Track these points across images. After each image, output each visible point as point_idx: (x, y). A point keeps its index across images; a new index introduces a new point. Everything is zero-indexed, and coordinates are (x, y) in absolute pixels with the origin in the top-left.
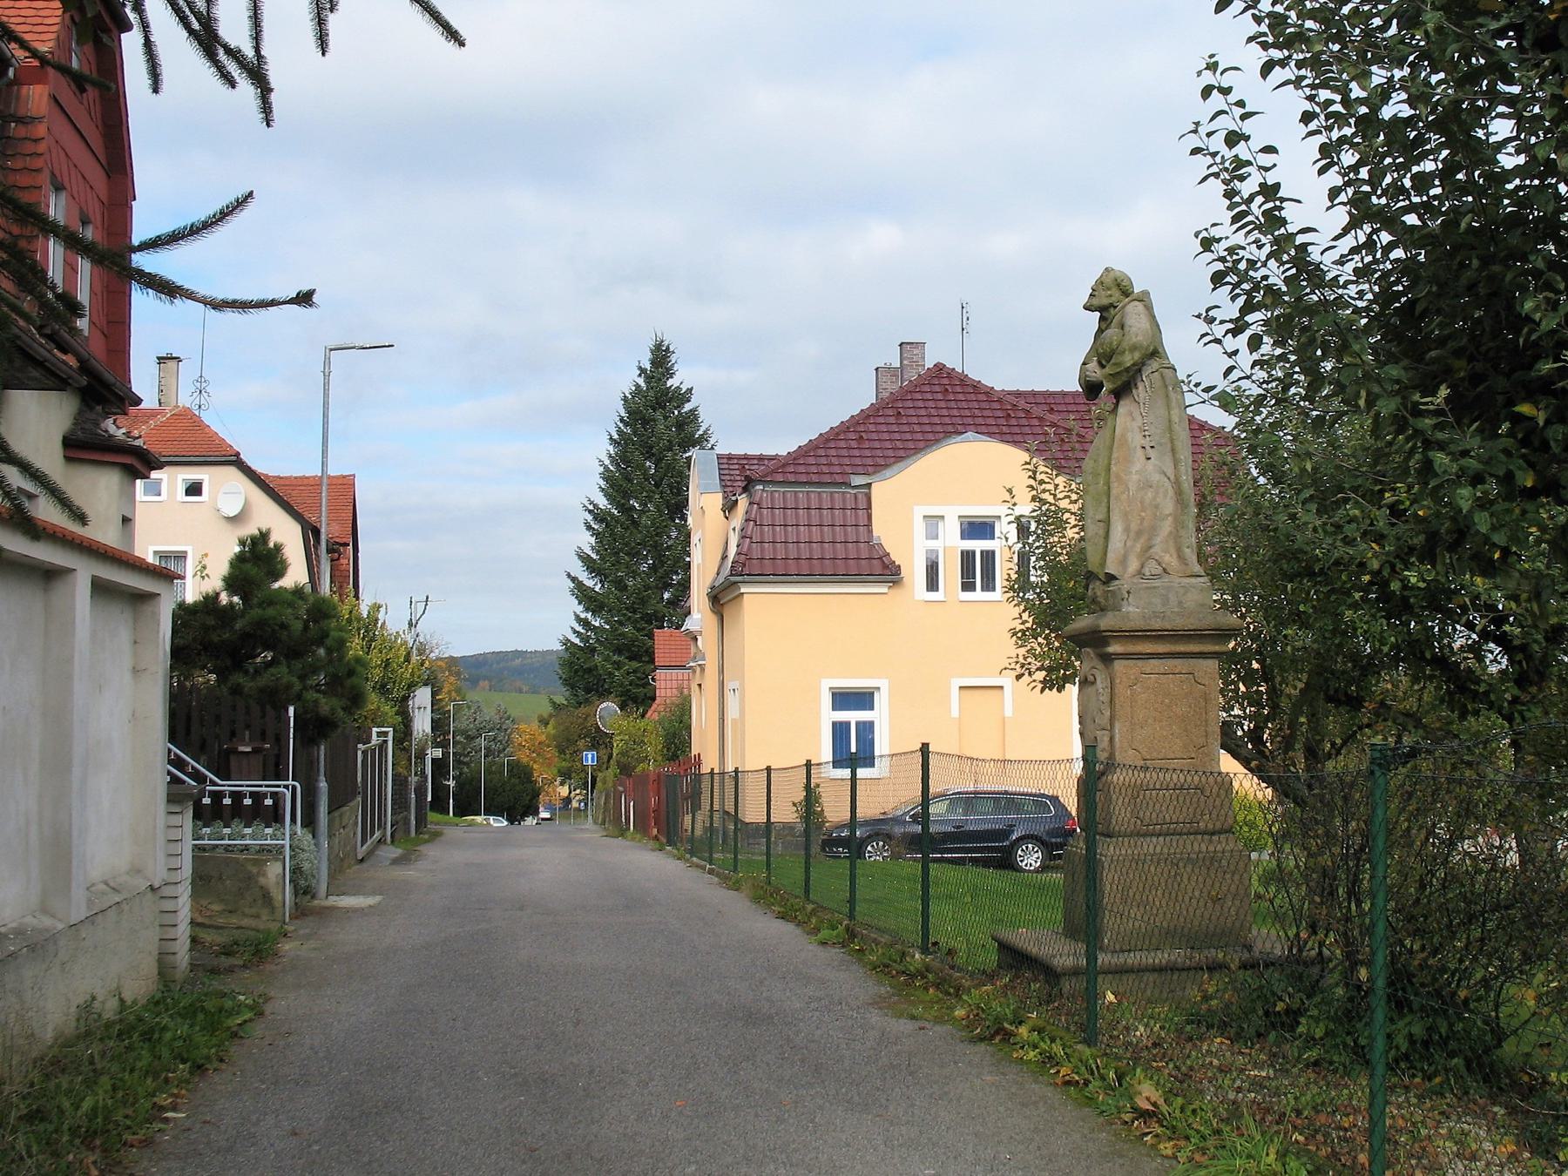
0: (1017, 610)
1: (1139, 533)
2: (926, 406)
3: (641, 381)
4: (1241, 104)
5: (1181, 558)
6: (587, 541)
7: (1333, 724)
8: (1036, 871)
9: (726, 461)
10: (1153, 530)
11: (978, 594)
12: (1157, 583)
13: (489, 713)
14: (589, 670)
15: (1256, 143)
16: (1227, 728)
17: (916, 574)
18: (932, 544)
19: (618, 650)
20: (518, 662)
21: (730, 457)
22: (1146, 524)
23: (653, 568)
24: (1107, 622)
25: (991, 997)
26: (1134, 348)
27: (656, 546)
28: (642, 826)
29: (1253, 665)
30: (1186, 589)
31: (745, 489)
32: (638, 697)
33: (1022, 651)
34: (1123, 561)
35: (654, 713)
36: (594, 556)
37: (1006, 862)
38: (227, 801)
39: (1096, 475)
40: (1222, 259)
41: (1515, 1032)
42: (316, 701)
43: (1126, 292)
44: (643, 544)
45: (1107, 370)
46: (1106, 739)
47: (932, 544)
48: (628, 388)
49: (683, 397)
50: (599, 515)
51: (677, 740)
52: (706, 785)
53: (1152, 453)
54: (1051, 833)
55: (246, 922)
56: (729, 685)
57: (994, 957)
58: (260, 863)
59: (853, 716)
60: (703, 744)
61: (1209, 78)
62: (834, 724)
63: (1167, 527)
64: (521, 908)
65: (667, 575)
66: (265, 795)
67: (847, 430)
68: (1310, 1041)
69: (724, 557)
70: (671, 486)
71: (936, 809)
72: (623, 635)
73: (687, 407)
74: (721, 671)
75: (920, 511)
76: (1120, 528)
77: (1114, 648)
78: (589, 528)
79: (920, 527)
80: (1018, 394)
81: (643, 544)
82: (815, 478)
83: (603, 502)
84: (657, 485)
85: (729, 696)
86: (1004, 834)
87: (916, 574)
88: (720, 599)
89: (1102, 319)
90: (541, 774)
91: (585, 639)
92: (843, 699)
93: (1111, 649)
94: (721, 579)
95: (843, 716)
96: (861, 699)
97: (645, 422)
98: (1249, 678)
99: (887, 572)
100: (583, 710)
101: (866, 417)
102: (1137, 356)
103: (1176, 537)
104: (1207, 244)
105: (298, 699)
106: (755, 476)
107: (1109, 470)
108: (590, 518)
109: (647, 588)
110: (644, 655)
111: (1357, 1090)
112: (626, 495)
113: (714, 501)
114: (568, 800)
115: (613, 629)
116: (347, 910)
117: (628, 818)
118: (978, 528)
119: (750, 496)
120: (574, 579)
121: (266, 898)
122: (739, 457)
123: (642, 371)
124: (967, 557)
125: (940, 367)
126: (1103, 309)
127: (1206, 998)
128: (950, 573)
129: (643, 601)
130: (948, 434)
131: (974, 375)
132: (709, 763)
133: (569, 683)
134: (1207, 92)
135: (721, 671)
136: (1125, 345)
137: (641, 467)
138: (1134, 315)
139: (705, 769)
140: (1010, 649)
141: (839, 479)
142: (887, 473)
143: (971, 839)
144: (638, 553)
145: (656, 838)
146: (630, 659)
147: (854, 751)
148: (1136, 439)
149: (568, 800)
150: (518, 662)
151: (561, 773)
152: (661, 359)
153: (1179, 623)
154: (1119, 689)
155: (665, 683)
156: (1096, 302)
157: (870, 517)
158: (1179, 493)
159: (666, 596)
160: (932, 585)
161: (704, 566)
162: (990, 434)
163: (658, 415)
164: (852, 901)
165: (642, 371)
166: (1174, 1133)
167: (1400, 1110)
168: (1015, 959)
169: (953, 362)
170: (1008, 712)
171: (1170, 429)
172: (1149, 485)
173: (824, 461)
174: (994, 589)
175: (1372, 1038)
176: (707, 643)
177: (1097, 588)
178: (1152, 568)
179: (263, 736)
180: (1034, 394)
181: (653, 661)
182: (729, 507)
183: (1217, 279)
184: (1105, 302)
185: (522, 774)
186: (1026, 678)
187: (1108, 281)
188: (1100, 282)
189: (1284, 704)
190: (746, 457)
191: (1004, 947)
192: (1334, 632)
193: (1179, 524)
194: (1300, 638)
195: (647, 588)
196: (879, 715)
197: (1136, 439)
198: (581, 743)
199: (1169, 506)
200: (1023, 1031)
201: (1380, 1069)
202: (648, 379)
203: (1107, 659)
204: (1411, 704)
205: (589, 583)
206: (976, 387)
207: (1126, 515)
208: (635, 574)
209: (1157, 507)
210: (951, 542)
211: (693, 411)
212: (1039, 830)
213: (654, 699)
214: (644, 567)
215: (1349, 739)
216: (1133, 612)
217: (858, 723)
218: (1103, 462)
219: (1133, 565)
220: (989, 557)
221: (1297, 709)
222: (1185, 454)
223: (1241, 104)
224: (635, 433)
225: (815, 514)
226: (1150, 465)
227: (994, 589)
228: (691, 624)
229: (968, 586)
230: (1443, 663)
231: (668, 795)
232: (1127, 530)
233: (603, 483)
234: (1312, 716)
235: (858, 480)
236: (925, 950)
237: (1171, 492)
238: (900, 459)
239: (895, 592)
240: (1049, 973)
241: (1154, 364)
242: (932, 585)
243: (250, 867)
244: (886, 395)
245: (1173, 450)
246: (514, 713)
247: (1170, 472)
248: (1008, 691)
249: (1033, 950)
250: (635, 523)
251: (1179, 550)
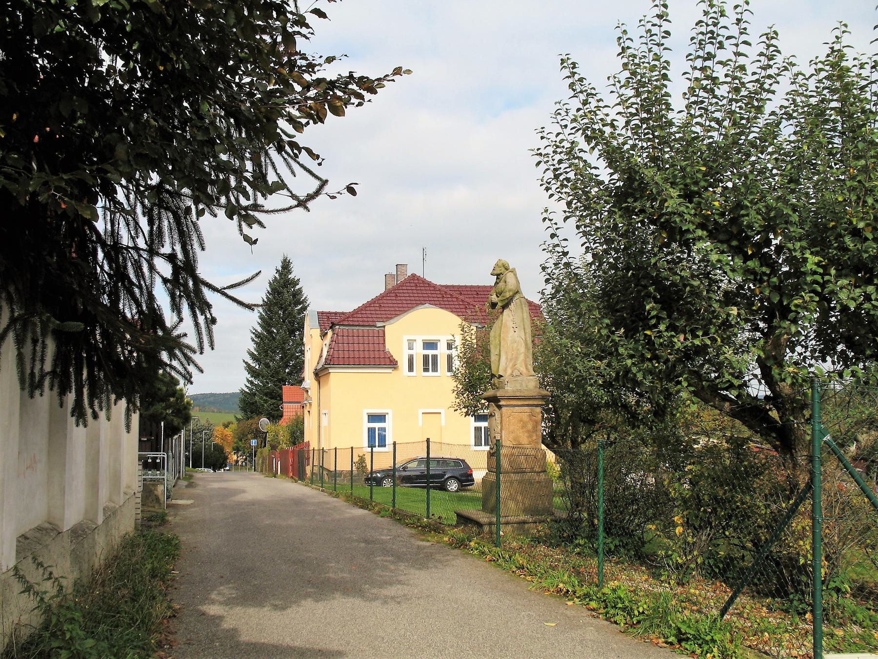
0: (455, 384)
1: (511, 360)
2: (408, 293)
3: (277, 276)
4: (556, 224)
5: (527, 368)
6: (252, 347)
7: (583, 429)
8: (457, 491)
9: (321, 315)
10: (517, 358)
11: (430, 373)
12: (518, 378)
13: (203, 422)
14: (253, 404)
15: (561, 238)
18: (411, 352)
19: (266, 395)
20: (212, 399)
21: (322, 313)
23: (281, 358)
24: (499, 394)
25: (459, 533)
26: (510, 291)
27: (283, 348)
28: (285, 471)
29: (552, 406)
30: (529, 381)
31: (331, 328)
32: (275, 416)
33: (458, 400)
34: (505, 370)
35: (284, 423)
36: (256, 353)
37: (443, 488)
38: (150, 461)
39: (495, 337)
40: (549, 274)
41: (649, 541)
42: (172, 420)
43: (507, 269)
44: (277, 347)
45: (500, 298)
47: (411, 352)
48: (271, 279)
49: (295, 283)
50: (258, 335)
51: (297, 433)
52: (311, 453)
53: (516, 330)
54: (462, 475)
55: (150, 509)
56: (323, 411)
57: (455, 518)
58: (155, 485)
59: (377, 425)
60: (310, 435)
61: (545, 215)
63: (522, 357)
64: (253, 505)
65: (288, 362)
66: (157, 458)
67: (374, 303)
68: (578, 545)
69: (321, 356)
70: (290, 322)
71: (433, 466)
72: (268, 388)
73: (297, 287)
74: (319, 405)
75: (405, 338)
77: (502, 403)
78: (253, 340)
80: (447, 287)
81: (277, 347)
82: (361, 323)
83: (259, 329)
84: (284, 321)
85: (323, 417)
86: (443, 476)
87: (404, 364)
88: (319, 375)
89: (497, 278)
90: (228, 449)
91: (251, 390)
92: (373, 418)
93: (501, 403)
94: (320, 366)
95: (372, 425)
96: (381, 418)
97: (279, 293)
98: (548, 411)
99: (392, 364)
100: (250, 421)
101: (382, 297)
102: (511, 293)
103: (525, 361)
104: (544, 269)
105: (164, 419)
106: (336, 322)
107: (500, 336)
108: (253, 336)
109: (279, 367)
110: (277, 397)
111: (594, 562)
112: (270, 326)
113: (317, 332)
114: (237, 461)
115: (264, 386)
116: (183, 505)
118: (430, 345)
119: (333, 330)
120: (246, 363)
121: (157, 499)
122: (327, 313)
123: (278, 271)
124: (426, 358)
125: (414, 275)
126: (498, 275)
127: (539, 531)
128: (418, 364)
129: (278, 373)
130: (418, 304)
131: (428, 279)
132: (314, 445)
133: (244, 409)
134: (544, 219)
135: (319, 405)
136: (507, 289)
137: (277, 313)
138: (510, 277)
139: (311, 448)
140: (452, 398)
141: (371, 323)
142: (392, 321)
143: (434, 475)
144: (275, 352)
145: (292, 477)
146: (271, 398)
147: (376, 438)
148: (511, 324)
149: (237, 461)
150: (212, 399)
151: (234, 449)
152: (286, 266)
153: (526, 394)
154: (504, 418)
155: (289, 410)
156: (495, 272)
157: (384, 340)
158: (526, 344)
159: (287, 370)
160: (411, 369)
161: (311, 359)
162: (435, 305)
163: (285, 291)
164: (394, 500)
165: (278, 271)
166: (531, 574)
167: (607, 567)
168: (463, 520)
169: (419, 274)
170: (443, 423)
173: (365, 316)
175: (599, 545)
176: (313, 393)
177: (495, 380)
178: (516, 373)
179: (151, 435)
180: (453, 286)
181: (281, 399)
182: (324, 335)
183: (547, 281)
184: (499, 272)
185: (219, 449)
186: (459, 411)
187: (500, 264)
188: (497, 265)
189: (563, 421)
190: (329, 313)
191: (459, 516)
192: (583, 395)
193: (526, 356)
194: (570, 398)
195: (279, 367)
196: (388, 425)
198: (249, 436)
199: (523, 350)
200: (472, 544)
201: (601, 555)
202: (280, 275)
203: (500, 407)
204: (614, 422)
205: (254, 365)
206: (429, 284)
208: (273, 360)
210: (419, 352)
211: (300, 289)
212: (457, 474)
213: (282, 416)
214: (278, 358)
215: (589, 436)
216: (510, 388)
218: (498, 332)
219: (509, 371)
220: (435, 357)
221: (567, 424)
222: (529, 330)
223: (556, 224)
224: (274, 298)
225: (359, 339)
228: (305, 385)
229: (426, 370)
230: (625, 407)
231: (296, 459)
232: (507, 358)
233: (259, 321)
234: (574, 427)
235: (379, 324)
236: (428, 517)
238: (397, 315)
239: (395, 372)
240: (479, 525)
241: (517, 296)
242: (411, 369)
243: (151, 487)
244: (390, 287)
246: (212, 422)
247: (523, 337)
248: (443, 414)
249: (474, 517)
250: (274, 339)
251: (526, 366)
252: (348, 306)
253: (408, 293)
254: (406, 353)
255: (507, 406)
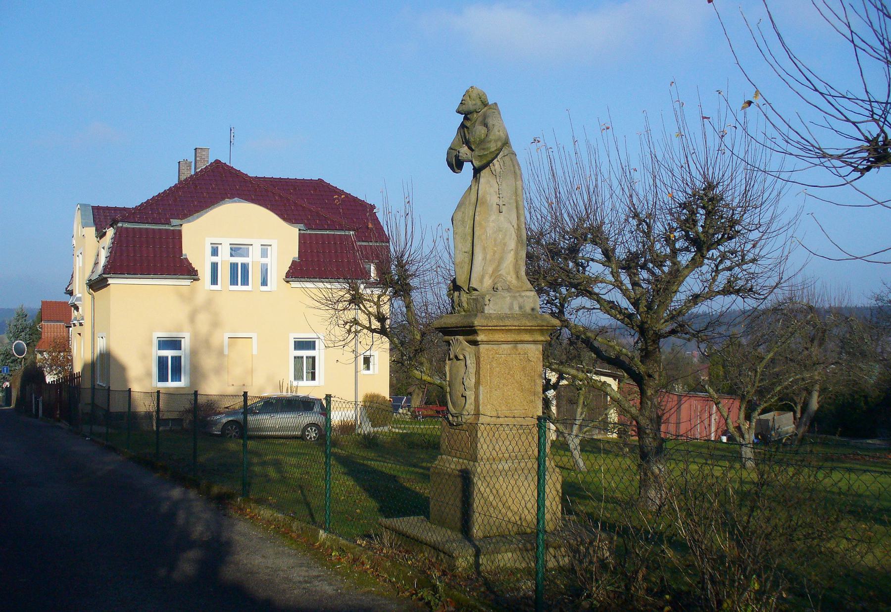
11: (239, 287)
16: (77, 308)
17: (205, 274)
18: (214, 259)
22: (497, 256)
34: (481, 281)
46: (473, 397)
47: (214, 259)
62: (159, 357)
69: (96, 264)
75: (274, 243)
76: (480, 258)
79: (208, 250)
87: (205, 274)
89: (466, 118)
99: (188, 271)
117: (37, 410)
124: (234, 266)
125: (217, 162)
128: (224, 274)
160: (214, 281)
170: (255, 352)
171: (516, 195)
172: (500, 230)
174: (248, 285)
182: (101, 235)
184: (472, 108)
197: (493, 200)
207: (484, 249)
209: (505, 244)
210: (224, 258)
217: (172, 357)
220: (245, 267)
226: (502, 217)
227: (248, 285)
229: (234, 281)
232: (484, 259)
237: (514, 236)
242: (214, 281)
244: (183, 178)
245: (517, 208)
247: (515, 223)
248: (255, 340)
252: (132, 200)
253: (212, 184)
254: (210, 259)
255: (488, 342)
